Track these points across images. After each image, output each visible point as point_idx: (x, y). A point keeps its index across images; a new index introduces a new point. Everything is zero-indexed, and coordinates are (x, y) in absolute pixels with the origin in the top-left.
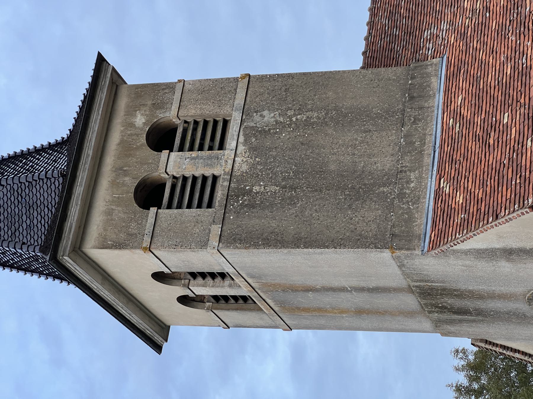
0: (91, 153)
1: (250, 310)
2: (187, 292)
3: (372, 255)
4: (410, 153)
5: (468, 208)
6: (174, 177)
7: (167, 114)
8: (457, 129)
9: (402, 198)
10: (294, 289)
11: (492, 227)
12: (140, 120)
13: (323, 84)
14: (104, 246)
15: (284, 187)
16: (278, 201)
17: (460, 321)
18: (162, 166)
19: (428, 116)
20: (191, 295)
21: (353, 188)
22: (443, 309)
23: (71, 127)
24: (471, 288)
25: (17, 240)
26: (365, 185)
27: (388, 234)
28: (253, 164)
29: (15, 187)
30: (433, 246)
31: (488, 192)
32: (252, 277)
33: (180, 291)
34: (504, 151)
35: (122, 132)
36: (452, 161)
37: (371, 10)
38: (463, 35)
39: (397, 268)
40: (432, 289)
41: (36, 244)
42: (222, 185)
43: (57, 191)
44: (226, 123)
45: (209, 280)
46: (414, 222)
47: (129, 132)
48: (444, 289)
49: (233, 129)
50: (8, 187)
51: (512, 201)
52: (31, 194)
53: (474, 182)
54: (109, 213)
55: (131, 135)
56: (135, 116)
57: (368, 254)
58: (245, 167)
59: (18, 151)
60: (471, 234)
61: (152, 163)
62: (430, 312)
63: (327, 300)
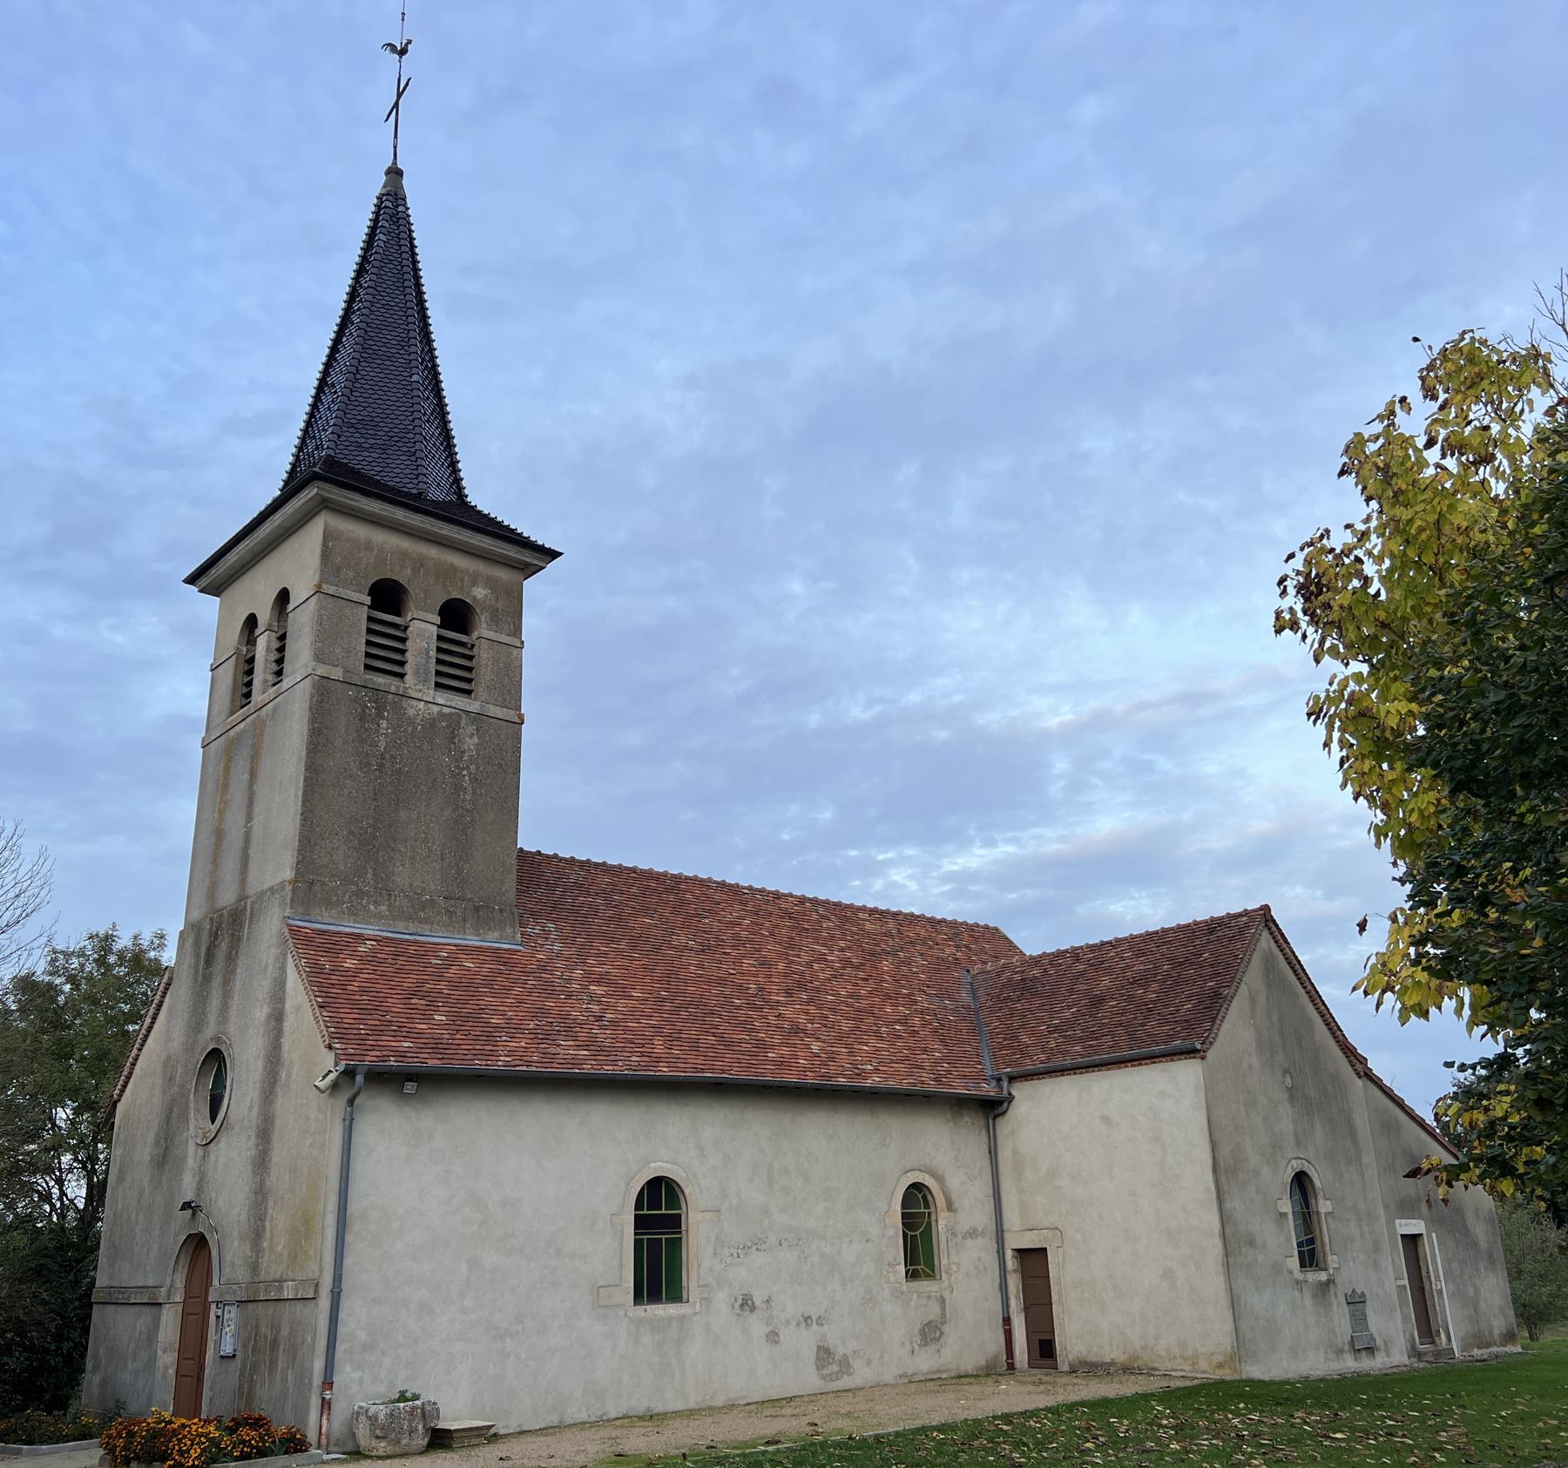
0: (444, 532)
1: (233, 700)
2: (261, 628)
3: (289, 857)
4: (412, 906)
5: (336, 973)
6: (406, 628)
7: (484, 625)
8: (434, 962)
9: (357, 895)
10: (255, 758)
11: (310, 1001)
12: (480, 593)
13: (503, 808)
14: (326, 526)
15: (383, 757)
16: (366, 748)
17: (197, 955)
18: (421, 615)
19: (454, 927)
20: (258, 632)
21: (375, 838)
22: (215, 936)
23: (479, 508)
24: (238, 970)
25: (345, 429)
26: (378, 852)
27: (315, 877)
28: (414, 723)
29: (411, 436)
30: (295, 932)
31: (353, 997)
32: (275, 710)
33: (264, 618)
34: (402, 1015)
35: (467, 570)
36: (396, 955)
37: (588, 861)
38: (543, 969)
39: (271, 885)
40: (241, 925)
41: (338, 451)
42: (391, 684)
43: (401, 485)
44: (468, 692)
45: (274, 656)
46: (326, 909)
47: (466, 579)
48: (239, 939)
49: (460, 701)
50: (411, 427)
51: (339, 1025)
52: (399, 453)
53: (368, 981)
54: (368, 546)
55: (462, 580)
56: (484, 588)
57: (291, 852)
58: (411, 712)
59: (455, 441)
60: (304, 976)
61: (426, 602)
62: (211, 919)
63: (238, 795)
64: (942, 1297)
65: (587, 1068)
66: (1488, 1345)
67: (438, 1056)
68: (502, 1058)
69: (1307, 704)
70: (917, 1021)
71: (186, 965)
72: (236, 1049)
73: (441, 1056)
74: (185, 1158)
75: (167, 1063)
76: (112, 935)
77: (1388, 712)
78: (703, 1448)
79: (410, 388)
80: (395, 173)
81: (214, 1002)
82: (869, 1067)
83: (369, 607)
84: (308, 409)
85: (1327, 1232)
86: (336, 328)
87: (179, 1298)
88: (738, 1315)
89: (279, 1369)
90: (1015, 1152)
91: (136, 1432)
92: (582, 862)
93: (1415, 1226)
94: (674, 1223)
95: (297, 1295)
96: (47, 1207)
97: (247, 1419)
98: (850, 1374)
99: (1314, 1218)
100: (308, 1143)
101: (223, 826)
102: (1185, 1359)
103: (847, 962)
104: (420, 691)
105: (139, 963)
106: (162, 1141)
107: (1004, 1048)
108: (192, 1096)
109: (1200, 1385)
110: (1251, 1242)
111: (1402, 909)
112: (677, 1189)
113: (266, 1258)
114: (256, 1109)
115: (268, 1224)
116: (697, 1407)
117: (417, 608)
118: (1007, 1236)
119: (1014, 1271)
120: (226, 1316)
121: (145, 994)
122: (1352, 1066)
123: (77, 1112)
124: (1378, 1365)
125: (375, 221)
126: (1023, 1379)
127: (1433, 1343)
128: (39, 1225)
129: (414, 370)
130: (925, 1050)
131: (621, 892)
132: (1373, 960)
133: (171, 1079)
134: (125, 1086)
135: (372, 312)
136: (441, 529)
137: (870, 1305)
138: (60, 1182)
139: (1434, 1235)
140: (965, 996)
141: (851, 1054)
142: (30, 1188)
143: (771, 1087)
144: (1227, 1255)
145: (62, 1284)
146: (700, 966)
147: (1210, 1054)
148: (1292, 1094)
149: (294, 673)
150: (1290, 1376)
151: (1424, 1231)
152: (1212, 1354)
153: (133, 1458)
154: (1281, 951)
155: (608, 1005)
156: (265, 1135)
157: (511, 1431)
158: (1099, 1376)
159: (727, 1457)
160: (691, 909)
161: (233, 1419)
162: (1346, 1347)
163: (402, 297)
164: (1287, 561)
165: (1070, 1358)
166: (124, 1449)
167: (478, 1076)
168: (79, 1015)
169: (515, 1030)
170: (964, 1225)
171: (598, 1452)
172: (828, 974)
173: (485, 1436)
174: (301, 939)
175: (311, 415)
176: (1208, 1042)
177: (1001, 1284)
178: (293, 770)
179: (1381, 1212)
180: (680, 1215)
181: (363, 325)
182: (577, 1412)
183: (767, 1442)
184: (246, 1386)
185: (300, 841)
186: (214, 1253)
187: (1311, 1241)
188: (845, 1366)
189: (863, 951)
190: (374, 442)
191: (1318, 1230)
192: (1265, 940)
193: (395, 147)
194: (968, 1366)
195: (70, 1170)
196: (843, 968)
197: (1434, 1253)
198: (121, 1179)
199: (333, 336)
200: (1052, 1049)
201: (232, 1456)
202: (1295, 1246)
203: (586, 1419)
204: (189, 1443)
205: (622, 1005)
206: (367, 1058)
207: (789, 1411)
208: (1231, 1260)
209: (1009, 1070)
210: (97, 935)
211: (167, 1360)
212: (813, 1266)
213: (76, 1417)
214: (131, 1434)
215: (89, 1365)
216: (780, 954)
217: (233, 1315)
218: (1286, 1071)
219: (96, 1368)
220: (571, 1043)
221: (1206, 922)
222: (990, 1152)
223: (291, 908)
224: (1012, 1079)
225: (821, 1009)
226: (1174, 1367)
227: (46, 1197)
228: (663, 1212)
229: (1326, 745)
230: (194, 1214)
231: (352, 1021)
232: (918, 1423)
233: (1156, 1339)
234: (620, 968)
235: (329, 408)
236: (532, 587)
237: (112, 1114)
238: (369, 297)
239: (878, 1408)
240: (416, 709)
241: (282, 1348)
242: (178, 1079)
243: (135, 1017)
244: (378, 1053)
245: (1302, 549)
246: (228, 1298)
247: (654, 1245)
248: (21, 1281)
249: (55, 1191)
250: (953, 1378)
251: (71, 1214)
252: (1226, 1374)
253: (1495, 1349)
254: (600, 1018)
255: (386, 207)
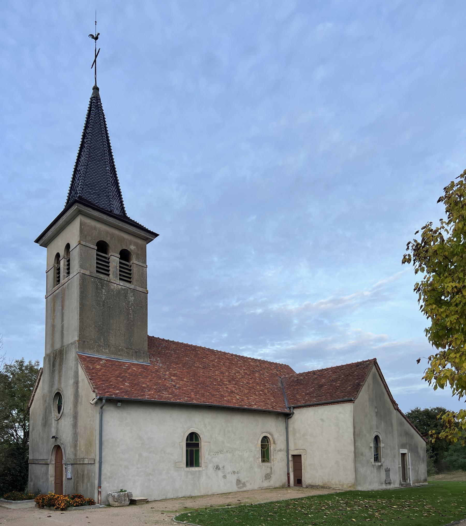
1: (54, 283)
3: (77, 333)
4: (116, 350)
5: (94, 369)
6: (109, 258)
7: (134, 259)
10: (63, 301)
11: (87, 377)
12: (132, 247)
15: (104, 302)
16: (99, 299)
17: (50, 364)
20: (60, 259)
22: (55, 358)
24: (63, 369)
25: (84, 186)
26: (104, 333)
27: (85, 340)
29: (107, 190)
30: (80, 357)
31: (100, 377)
32: (68, 285)
33: (62, 254)
35: (128, 239)
36: (112, 365)
37: (168, 340)
38: (157, 371)
39: (71, 342)
40: (63, 354)
42: (105, 277)
43: (105, 208)
44: (130, 282)
45: (66, 267)
47: (128, 242)
48: (63, 359)
49: (127, 285)
54: (95, 228)
56: (134, 246)
58: (112, 287)
60: (84, 370)
63: (58, 314)
64: (271, 467)
65: (172, 400)
66: (419, 482)
67: (127, 395)
68: (146, 397)
69: (415, 286)
70: (266, 391)
71: (47, 368)
72: (65, 392)
73: (128, 395)
74: (52, 424)
75: (44, 396)
76: (23, 361)
77: (448, 286)
78: (209, 506)
79: (106, 172)
80: (96, 89)
81: (56, 378)
82: (253, 403)
83: (97, 250)
84: (71, 180)
85: (382, 452)
86: (79, 149)
87: (54, 462)
88: (215, 471)
89: (85, 482)
90: (294, 428)
91: (45, 499)
92: (166, 340)
93: (405, 451)
94: (197, 445)
95: (89, 462)
96: (13, 438)
97: (77, 495)
98: (245, 487)
99: (379, 448)
100: (89, 420)
101: (54, 324)
102: (340, 485)
103: (246, 374)
104: (115, 280)
105: (31, 369)
106: (45, 419)
107: (292, 399)
108: (52, 406)
109: (345, 492)
110: (362, 454)
111: (433, 356)
112: (197, 435)
113: (79, 452)
114: (72, 410)
115: (78, 443)
116: (203, 495)
117: (112, 252)
118: (290, 451)
119: (291, 461)
120: (68, 468)
121: (35, 379)
122: (394, 406)
123: (18, 412)
124: (391, 487)
125: (90, 108)
126: (294, 489)
127: (405, 482)
128: (11, 442)
129: (107, 166)
130: (269, 399)
131: (179, 350)
132: (427, 370)
133: (45, 401)
134: (31, 403)
135: (91, 143)
136: (119, 223)
137: (252, 469)
138: (16, 431)
139: (409, 453)
140: (279, 384)
141: (248, 399)
142: (7, 433)
143: (225, 408)
144: (355, 457)
145: (19, 458)
146: (203, 373)
147: (355, 401)
148: (377, 413)
149: (73, 272)
150: (369, 490)
151: (407, 452)
152: (348, 484)
153: (45, 505)
154: (378, 372)
155: (177, 383)
156: (75, 417)
157: (152, 500)
158: (315, 489)
159: (218, 509)
160: (200, 356)
161: (73, 496)
162: (384, 483)
163: (101, 137)
164: (415, 234)
165: (306, 484)
166: (42, 503)
167: (140, 402)
168: (16, 384)
169: (150, 389)
170: (278, 448)
171: (179, 507)
172: (240, 376)
173: (146, 501)
174: (83, 359)
175: (73, 182)
176: (355, 398)
177: (287, 464)
178: (76, 305)
179: (397, 447)
180: (199, 443)
181: (88, 147)
182: (170, 496)
183: (227, 505)
184: (75, 487)
185: (79, 328)
186: (63, 451)
187: (377, 454)
188: (244, 485)
189: (250, 370)
190: (95, 191)
191: (379, 451)
192: (374, 369)
193: (96, 78)
194: (278, 485)
195: (18, 428)
196: (245, 375)
197: (409, 458)
198: (33, 429)
199: (78, 152)
200: (306, 400)
201: (74, 505)
202: (373, 456)
203: (173, 497)
204: (61, 502)
205: (181, 383)
206: (106, 395)
207: (230, 497)
208: (356, 459)
209: (293, 405)
210: (18, 361)
211: (52, 479)
212: (236, 458)
213: (27, 494)
214: (43, 499)
215: (29, 479)
216: (226, 370)
217: (70, 468)
218: (376, 407)
219: (31, 481)
220: (167, 393)
221: (356, 363)
222: (286, 428)
223: (78, 349)
224: (294, 408)
225: (239, 386)
226: (337, 487)
227: (12, 435)
228: (194, 442)
229: (419, 300)
230: (56, 439)
231: (100, 384)
232: (269, 501)
233: (332, 480)
234: (180, 372)
235: (79, 179)
236: (150, 247)
237: (29, 411)
238: (90, 137)
239: (256, 496)
240: (113, 286)
241: (85, 477)
242: (47, 401)
243: (32, 385)
244: (109, 394)
245: (422, 229)
246: (68, 463)
247: (192, 451)
248: (8, 457)
249: (15, 433)
250: (273, 488)
251: (20, 440)
252: (352, 489)
253: (421, 484)
254: (175, 386)
255: (93, 110)
